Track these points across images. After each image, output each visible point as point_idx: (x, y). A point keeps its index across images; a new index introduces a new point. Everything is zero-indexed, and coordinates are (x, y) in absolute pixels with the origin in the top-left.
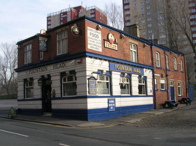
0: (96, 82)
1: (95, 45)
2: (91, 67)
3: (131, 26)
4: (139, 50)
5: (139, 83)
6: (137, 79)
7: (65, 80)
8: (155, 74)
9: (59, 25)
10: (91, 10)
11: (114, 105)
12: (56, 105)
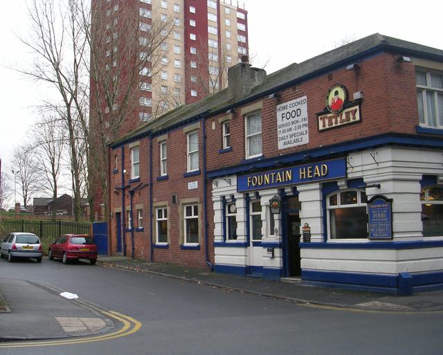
6: (317, 195)
7: (333, 202)
12: (311, 260)
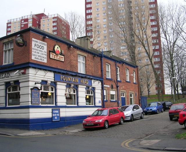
0: (39, 92)
1: (39, 56)
2: (34, 77)
3: (82, 37)
4: (87, 62)
5: (87, 93)
6: (84, 90)
7: (9, 91)
8: (105, 86)
9: (6, 35)
10: (54, 18)
11: (58, 115)
